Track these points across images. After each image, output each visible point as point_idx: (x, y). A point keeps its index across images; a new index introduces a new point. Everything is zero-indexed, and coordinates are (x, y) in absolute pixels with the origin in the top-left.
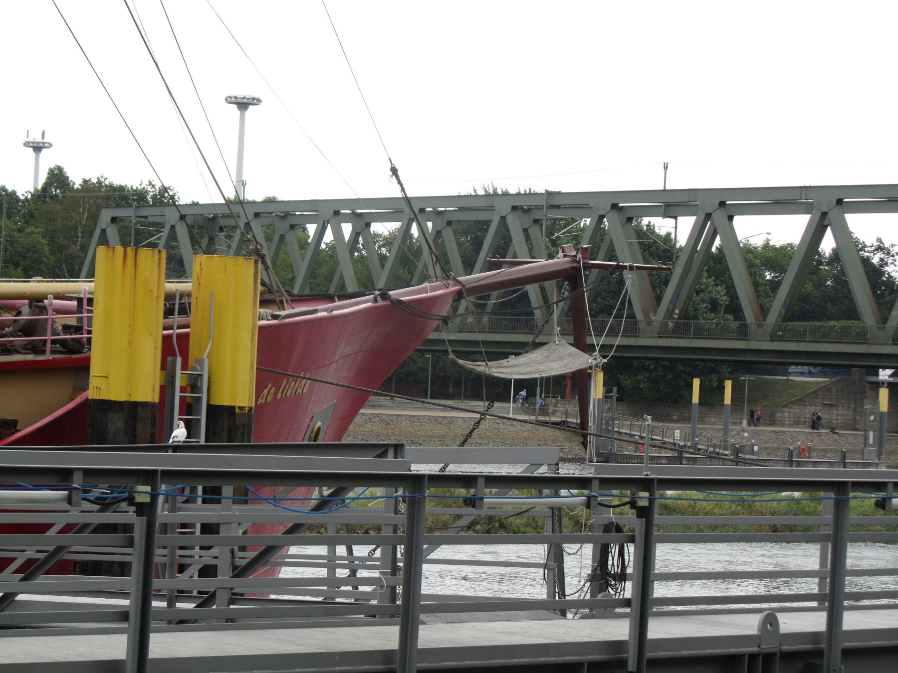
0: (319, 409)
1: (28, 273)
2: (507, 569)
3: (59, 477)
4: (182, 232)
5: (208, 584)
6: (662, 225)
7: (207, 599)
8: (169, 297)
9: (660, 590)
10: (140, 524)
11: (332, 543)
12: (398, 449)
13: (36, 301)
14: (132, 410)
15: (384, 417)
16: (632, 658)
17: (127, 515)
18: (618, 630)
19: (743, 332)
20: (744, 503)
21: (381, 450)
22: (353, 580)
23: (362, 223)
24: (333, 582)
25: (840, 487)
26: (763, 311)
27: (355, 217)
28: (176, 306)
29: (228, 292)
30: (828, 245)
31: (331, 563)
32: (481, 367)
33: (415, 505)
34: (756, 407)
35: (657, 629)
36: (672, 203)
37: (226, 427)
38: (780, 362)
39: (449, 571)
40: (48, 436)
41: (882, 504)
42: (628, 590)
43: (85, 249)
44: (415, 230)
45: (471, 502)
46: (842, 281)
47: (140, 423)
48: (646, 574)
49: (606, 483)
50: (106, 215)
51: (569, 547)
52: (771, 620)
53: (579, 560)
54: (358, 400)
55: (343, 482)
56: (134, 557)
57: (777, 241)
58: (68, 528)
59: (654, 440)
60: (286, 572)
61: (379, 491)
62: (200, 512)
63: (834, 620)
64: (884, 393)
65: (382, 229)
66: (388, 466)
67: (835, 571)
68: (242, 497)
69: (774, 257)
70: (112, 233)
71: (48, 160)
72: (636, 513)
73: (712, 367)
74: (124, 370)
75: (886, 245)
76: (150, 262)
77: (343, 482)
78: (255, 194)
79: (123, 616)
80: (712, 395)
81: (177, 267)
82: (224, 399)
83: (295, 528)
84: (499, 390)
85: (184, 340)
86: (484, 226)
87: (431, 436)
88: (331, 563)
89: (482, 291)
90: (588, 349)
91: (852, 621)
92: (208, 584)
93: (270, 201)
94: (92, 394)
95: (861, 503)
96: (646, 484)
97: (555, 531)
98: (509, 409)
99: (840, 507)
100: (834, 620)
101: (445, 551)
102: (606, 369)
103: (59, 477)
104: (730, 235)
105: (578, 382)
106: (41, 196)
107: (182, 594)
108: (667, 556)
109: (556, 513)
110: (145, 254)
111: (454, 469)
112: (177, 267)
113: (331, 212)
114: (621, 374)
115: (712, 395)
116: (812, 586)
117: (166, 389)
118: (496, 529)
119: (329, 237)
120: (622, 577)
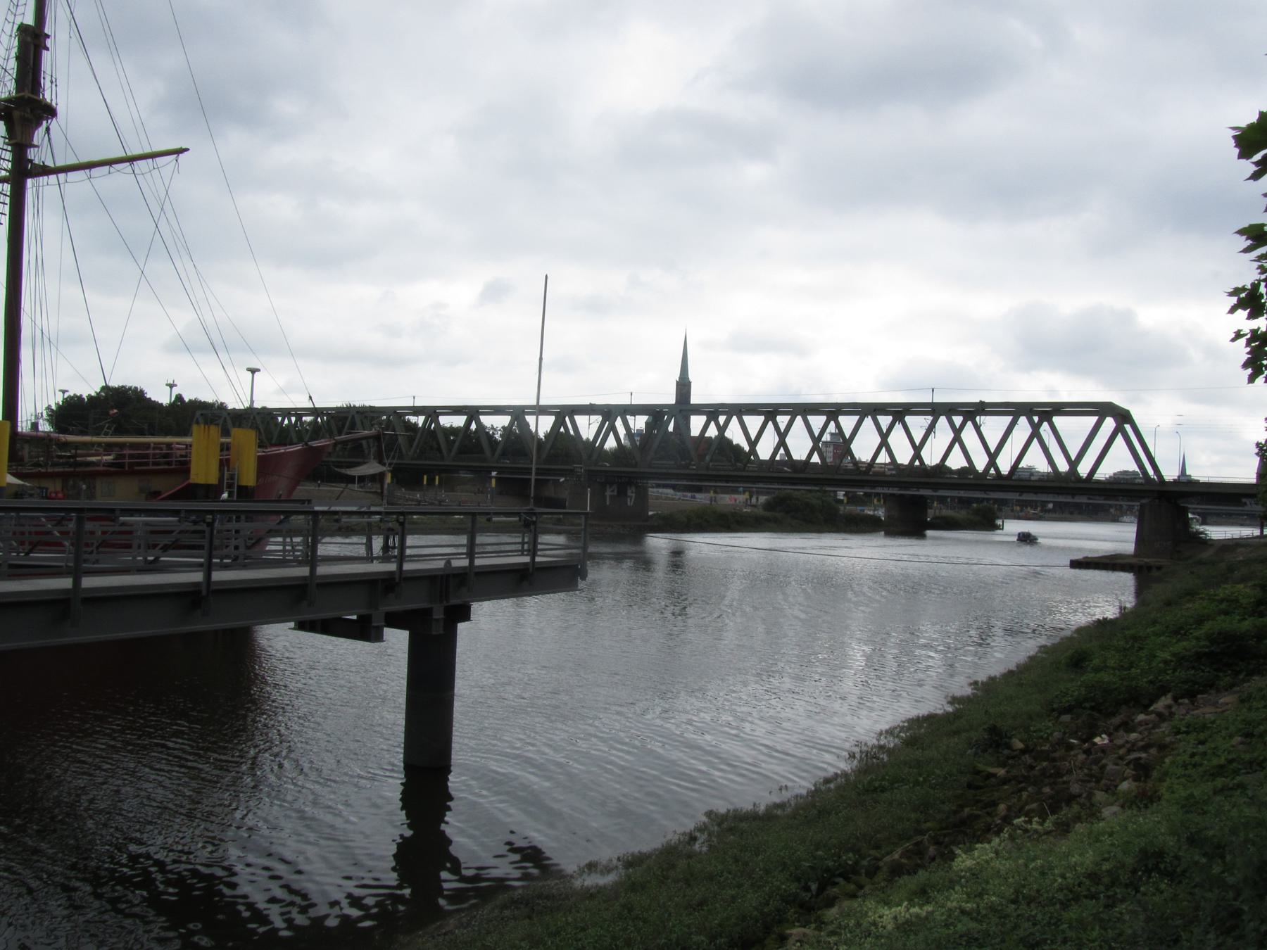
0: (281, 486)
1: (166, 434)
2: (352, 546)
3: (176, 513)
4: (229, 422)
5: (236, 553)
6: (413, 419)
7: (236, 559)
8: (222, 444)
9: (408, 552)
10: (207, 530)
11: (284, 537)
12: (309, 501)
13: (169, 445)
14: (207, 487)
15: (305, 489)
16: (397, 577)
17: (203, 527)
18: (392, 567)
19: (442, 458)
20: (441, 522)
21: (303, 502)
22: (294, 550)
23: (299, 417)
24: (284, 551)
25: (474, 515)
26: (450, 451)
28: (225, 448)
29: (245, 440)
30: (473, 426)
31: (284, 544)
32: (343, 471)
33: (316, 522)
34: (448, 484)
35: (538, 559)
36: (417, 411)
37: (244, 493)
38: (456, 469)
39: (330, 547)
40: (173, 497)
41: (489, 520)
42: (396, 552)
43: (190, 425)
45: (337, 521)
46: (478, 439)
47: (210, 492)
48: (403, 546)
49: (388, 513)
50: (198, 413)
51: (374, 537)
52: (448, 562)
53: (378, 543)
54: (295, 483)
55: (288, 514)
56: (205, 542)
57: (455, 425)
58: (181, 532)
59: (408, 498)
60: (268, 548)
61: (301, 517)
62: (233, 525)
63: (472, 562)
64: (493, 481)
65: (308, 419)
66: (305, 508)
67: (471, 545)
68: (248, 520)
69: (453, 431)
70: (201, 420)
71: (176, 391)
72: (399, 525)
73: (431, 472)
74: (204, 471)
75: (668, 397)
76: (214, 431)
77: (288, 514)
78: (257, 405)
79: (201, 565)
80: (431, 481)
81: (226, 433)
82: (244, 483)
83: (270, 531)
84: (351, 480)
85: (228, 460)
86: (346, 418)
87: (324, 498)
88: (284, 544)
89: (344, 443)
90: (384, 464)
91: (478, 562)
92: (236, 553)
93: (264, 408)
94: (191, 481)
95: (482, 520)
96: (402, 514)
97: (369, 531)
98: (356, 486)
99: (473, 522)
100: (472, 562)
101: (327, 539)
102: (392, 472)
103: (176, 513)
104: (438, 423)
105: (379, 478)
106: (172, 405)
107: (227, 557)
108: (410, 540)
109: (369, 524)
110: (213, 428)
111: (333, 509)
112: (226, 433)
113: (287, 412)
115: (431, 481)
116: (464, 551)
117: (221, 479)
118: (348, 531)
119: (286, 422)
120: (394, 548)
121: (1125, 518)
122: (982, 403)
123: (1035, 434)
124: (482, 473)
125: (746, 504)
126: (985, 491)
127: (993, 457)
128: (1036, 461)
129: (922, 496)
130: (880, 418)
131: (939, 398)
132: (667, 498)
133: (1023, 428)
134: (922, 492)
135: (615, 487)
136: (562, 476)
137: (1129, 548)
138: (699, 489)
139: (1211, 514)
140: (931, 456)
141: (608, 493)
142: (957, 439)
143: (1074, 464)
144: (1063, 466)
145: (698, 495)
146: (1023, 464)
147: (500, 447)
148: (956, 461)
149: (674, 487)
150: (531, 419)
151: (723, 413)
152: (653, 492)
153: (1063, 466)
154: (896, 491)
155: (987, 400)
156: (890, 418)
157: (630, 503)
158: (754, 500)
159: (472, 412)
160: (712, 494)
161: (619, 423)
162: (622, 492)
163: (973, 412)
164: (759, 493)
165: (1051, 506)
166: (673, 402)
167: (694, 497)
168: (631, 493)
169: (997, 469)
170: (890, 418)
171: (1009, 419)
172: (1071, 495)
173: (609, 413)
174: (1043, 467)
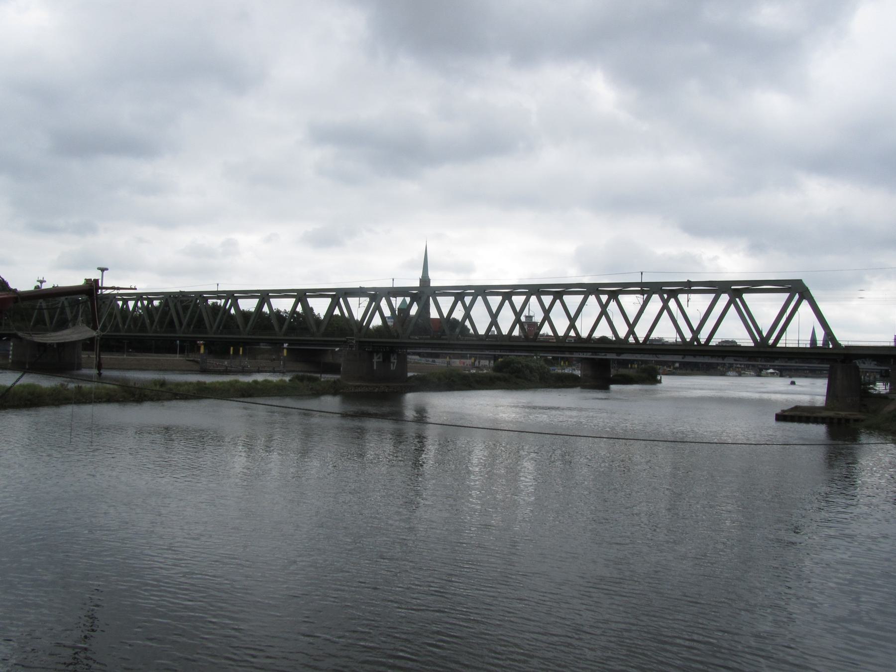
23: (151, 301)
26: (281, 328)
27: (148, 299)
30: (266, 309)
38: (258, 342)
44: (139, 304)
64: (285, 351)
65: (156, 303)
73: (236, 344)
75: (413, 281)
80: (236, 352)
114: (140, 314)
121: (729, 373)
122: (689, 282)
123: (665, 307)
124: (277, 344)
125: (473, 366)
126: (695, 356)
127: (631, 326)
128: (666, 332)
129: (607, 360)
130: (393, 299)
131: (647, 279)
132: (417, 363)
133: (656, 303)
134: (609, 356)
135: (380, 355)
136: (337, 346)
137: (820, 400)
138: (437, 356)
139: (787, 370)
140: (584, 328)
141: (375, 360)
142: (604, 312)
143: (696, 333)
144: (688, 335)
145: (437, 360)
146: (654, 336)
147: (286, 323)
148: (603, 331)
149: (419, 354)
150: (312, 302)
151: (469, 294)
152: (411, 358)
153: (688, 335)
154: (588, 355)
155: (692, 280)
156: (551, 298)
157: (393, 367)
158: (477, 363)
159: (264, 296)
160: (448, 359)
161: (384, 303)
162: (386, 360)
163: (670, 291)
164: (482, 357)
165: (677, 365)
166: (431, 285)
167: (434, 361)
168: (394, 359)
169: (636, 338)
170: (551, 298)
171: (581, 297)
172: (765, 357)
173: (375, 295)
174: (609, 335)
